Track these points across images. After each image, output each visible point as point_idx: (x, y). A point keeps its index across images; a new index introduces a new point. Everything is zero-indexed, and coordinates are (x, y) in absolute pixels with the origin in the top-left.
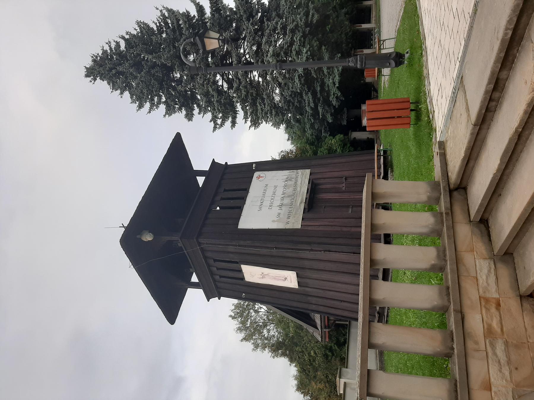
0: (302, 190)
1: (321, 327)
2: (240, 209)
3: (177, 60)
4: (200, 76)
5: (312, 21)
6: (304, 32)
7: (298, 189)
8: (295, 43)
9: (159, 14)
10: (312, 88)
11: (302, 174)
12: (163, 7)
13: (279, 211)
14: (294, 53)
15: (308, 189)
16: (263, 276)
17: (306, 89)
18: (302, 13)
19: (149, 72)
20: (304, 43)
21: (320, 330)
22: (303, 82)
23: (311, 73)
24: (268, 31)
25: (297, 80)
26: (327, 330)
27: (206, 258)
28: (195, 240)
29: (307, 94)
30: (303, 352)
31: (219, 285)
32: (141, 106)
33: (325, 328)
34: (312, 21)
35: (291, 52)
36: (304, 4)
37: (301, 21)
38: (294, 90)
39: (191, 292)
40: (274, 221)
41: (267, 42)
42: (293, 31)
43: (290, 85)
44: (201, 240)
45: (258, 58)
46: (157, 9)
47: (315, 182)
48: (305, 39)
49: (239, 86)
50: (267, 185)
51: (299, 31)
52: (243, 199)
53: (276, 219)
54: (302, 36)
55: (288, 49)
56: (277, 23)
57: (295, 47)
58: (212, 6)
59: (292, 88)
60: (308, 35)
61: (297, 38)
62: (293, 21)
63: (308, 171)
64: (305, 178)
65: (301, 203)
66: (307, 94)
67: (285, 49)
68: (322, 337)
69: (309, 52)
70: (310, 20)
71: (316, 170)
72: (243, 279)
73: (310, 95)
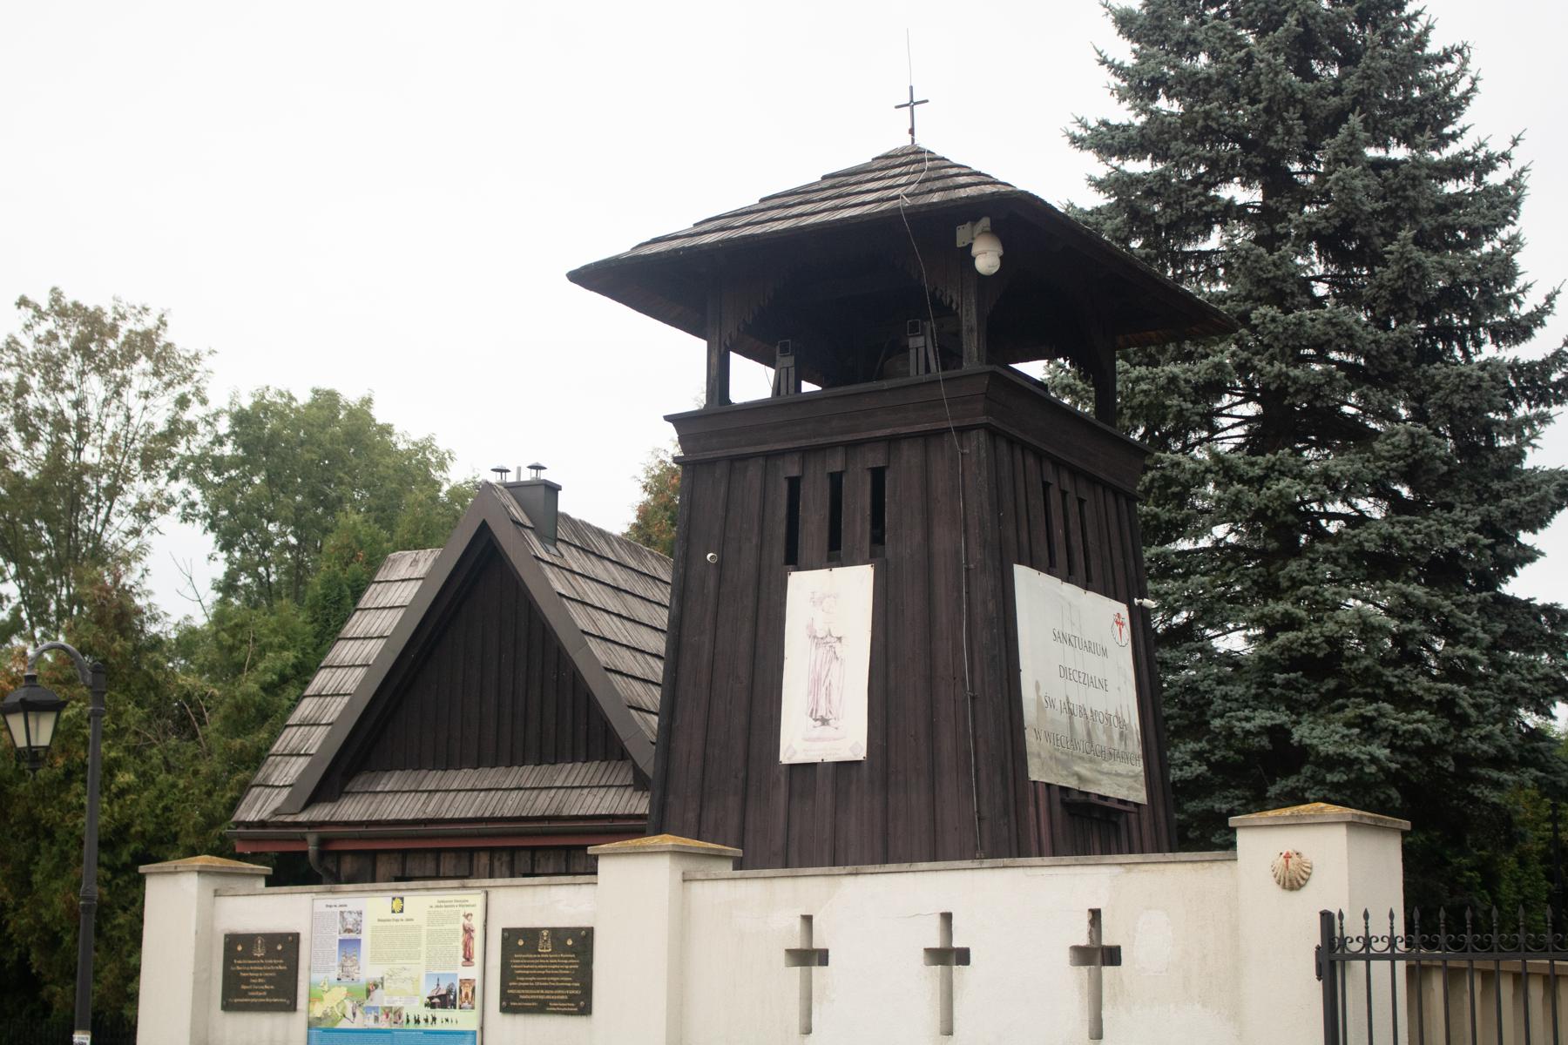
0: (1105, 780)
1: (323, 824)
4: (1281, 317)
5: (1477, 780)
6: (1440, 749)
7: (1106, 766)
8: (1403, 715)
9: (1496, 148)
10: (1218, 780)
11: (1136, 776)
12: (1523, 170)
13: (1057, 704)
14: (1369, 710)
15: (1106, 798)
16: (827, 641)
17: (1218, 755)
18: (1503, 741)
19: (1291, 99)
21: (302, 818)
22: (1254, 742)
24: (1447, 606)
25: (1263, 718)
26: (312, 848)
27: (893, 441)
28: (983, 419)
29: (1198, 756)
31: (754, 471)
32: (1125, 22)
33: (323, 842)
34: (1477, 780)
36: (1534, 750)
37: (1482, 739)
38: (1218, 705)
39: (695, 349)
40: (1038, 687)
41: (1409, 604)
42: (1446, 706)
43: (1238, 690)
44: (979, 439)
45: (1344, 560)
46: (1515, 143)
48: (1418, 752)
49: (1241, 480)
50: (1105, 652)
51: (1444, 730)
52: (1068, 578)
54: (1427, 740)
55: (1377, 685)
56: (1473, 642)
57: (1391, 716)
58: (1520, 367)
59: (1225, 697)
60: (1430, 763)
61: (1422, 721)
62: (1479, 707)
63: (1141, 796)
65: (1080, 778)
66: (1198, 756)
67: (1380, 675)
68: (262, 824)
69: (1373, 769)
70: (1483, 772)
71: (1145, 815)
72: (794, 560)
73: (1200, 769)
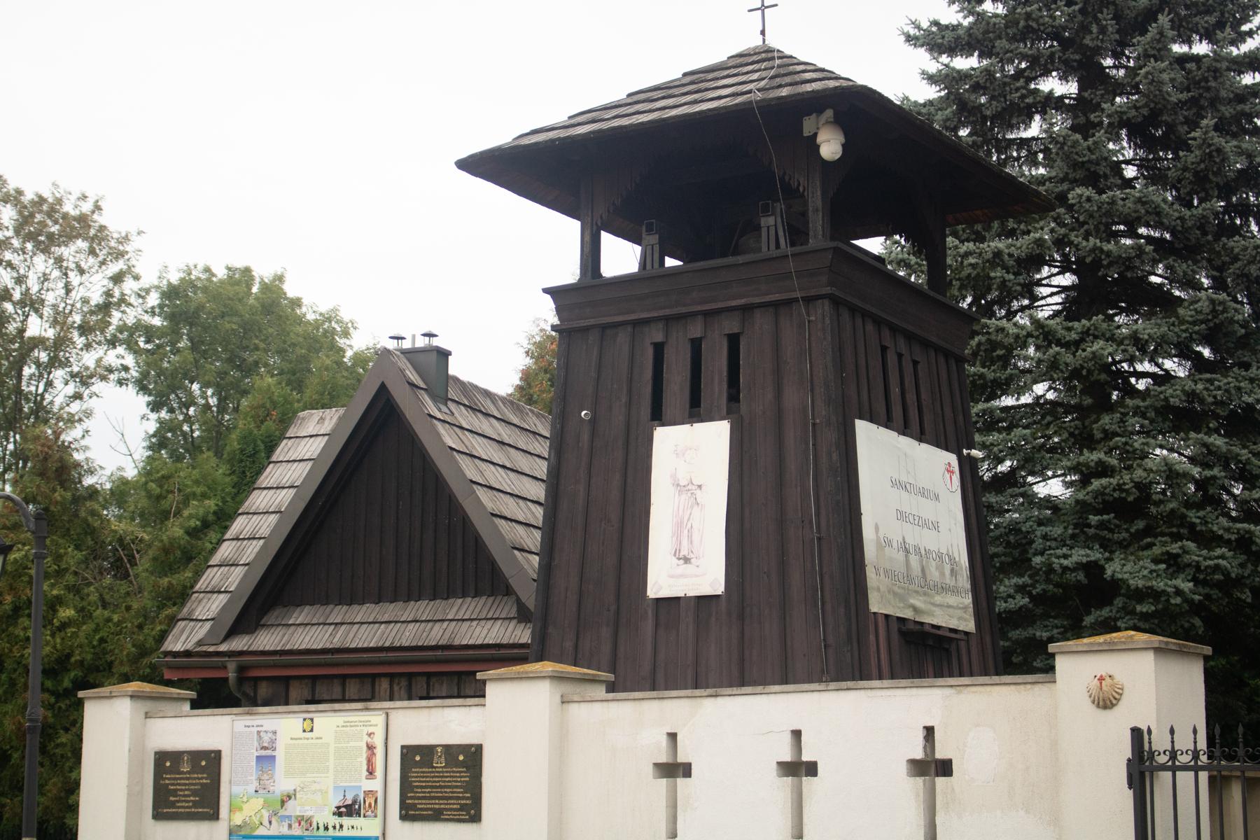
0: (938, 611)
1: (241, 653)
2: (887, 423)
3: (1145, 112)
4: (1096, 197)
6: (1239, 582)
7: (938, 599)
8: (1205, 552)
10: (1039, 611)
11: (965, 608)
13: (895, 545)
14: (1175, 548)
15: (938, 627)
16: (689, 489)
17: (1039, 589)
20: (1204, 583)
21: (223, 648)
23: (1100, 606)
25: (1079, 555)
26: (232, 675)
28: (827, 290)
29: (1021, 589)
30: (60, 573)
31: (623, 337)
33: (241, 669)
35: (1177, 537)
38: (1038, 544)
40: (877, 528)
41: (1210, 452)
43: (1057, 531)
45: (1151, 414)
47: (953, 646)
50: (937, 498)
51: (1242, 565)
52: (904, 430)
53: (881, 535)
54: (1226, 574)
55: (1182, 525)
57: (1193, 552)
61: (1222, 557)
63: (970, 626)
64: (960, 618)
65: (915, 609)
66: (1021, 589)
67: (1184, 517)
68: (187, 653)
69: (1178, 600)
72: (659, 416)
